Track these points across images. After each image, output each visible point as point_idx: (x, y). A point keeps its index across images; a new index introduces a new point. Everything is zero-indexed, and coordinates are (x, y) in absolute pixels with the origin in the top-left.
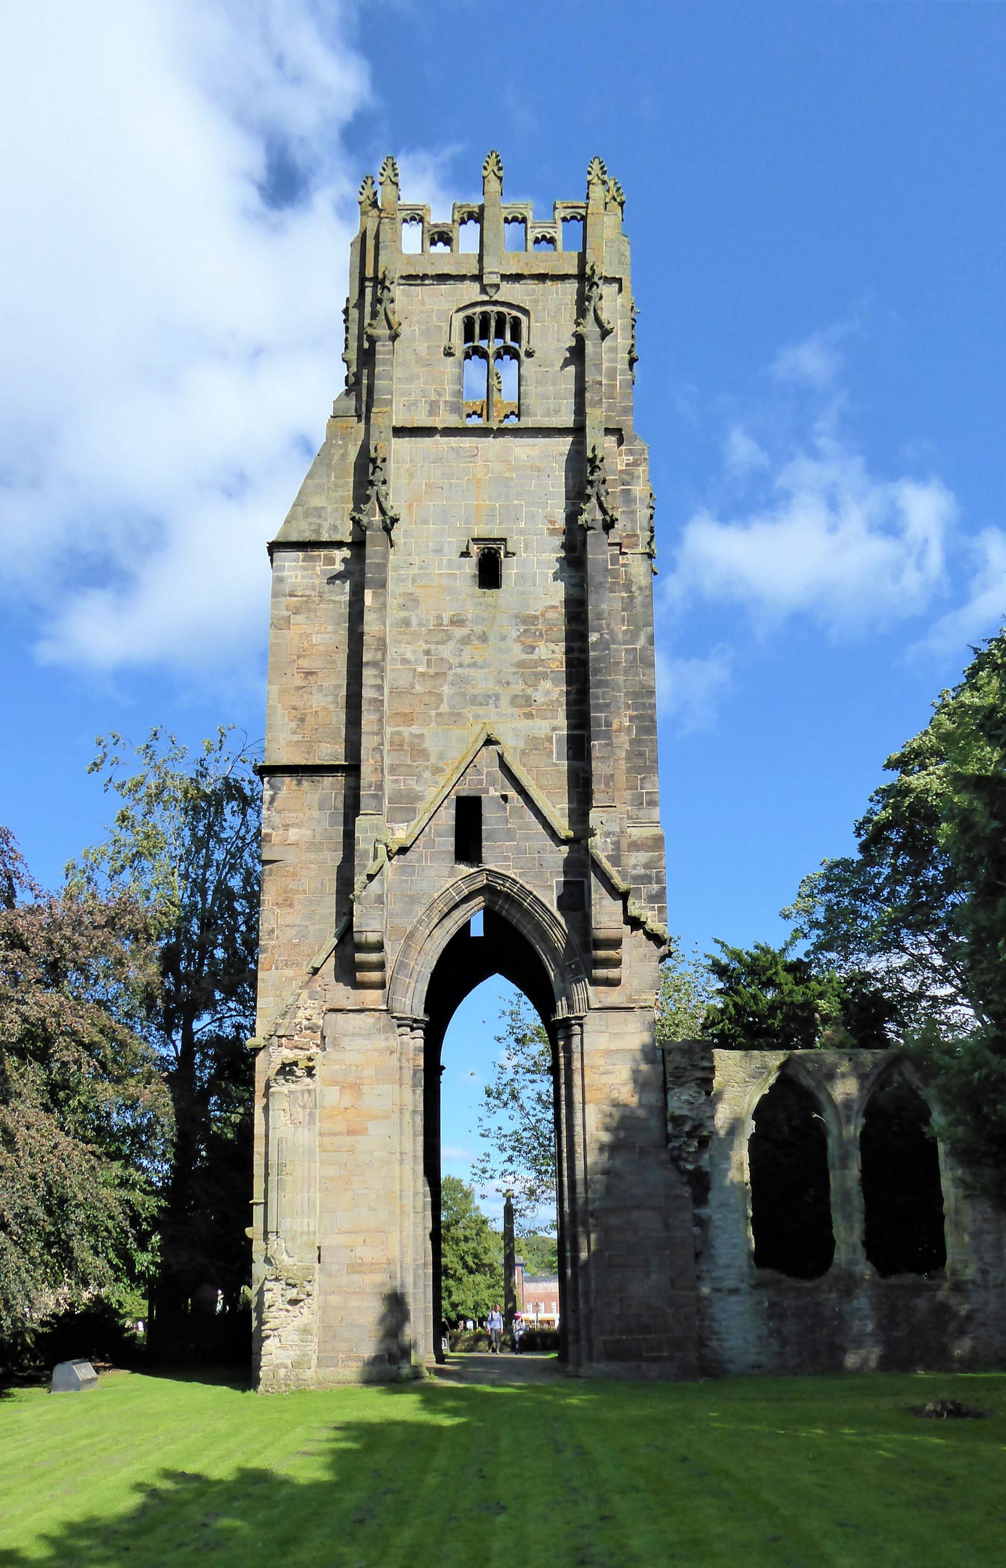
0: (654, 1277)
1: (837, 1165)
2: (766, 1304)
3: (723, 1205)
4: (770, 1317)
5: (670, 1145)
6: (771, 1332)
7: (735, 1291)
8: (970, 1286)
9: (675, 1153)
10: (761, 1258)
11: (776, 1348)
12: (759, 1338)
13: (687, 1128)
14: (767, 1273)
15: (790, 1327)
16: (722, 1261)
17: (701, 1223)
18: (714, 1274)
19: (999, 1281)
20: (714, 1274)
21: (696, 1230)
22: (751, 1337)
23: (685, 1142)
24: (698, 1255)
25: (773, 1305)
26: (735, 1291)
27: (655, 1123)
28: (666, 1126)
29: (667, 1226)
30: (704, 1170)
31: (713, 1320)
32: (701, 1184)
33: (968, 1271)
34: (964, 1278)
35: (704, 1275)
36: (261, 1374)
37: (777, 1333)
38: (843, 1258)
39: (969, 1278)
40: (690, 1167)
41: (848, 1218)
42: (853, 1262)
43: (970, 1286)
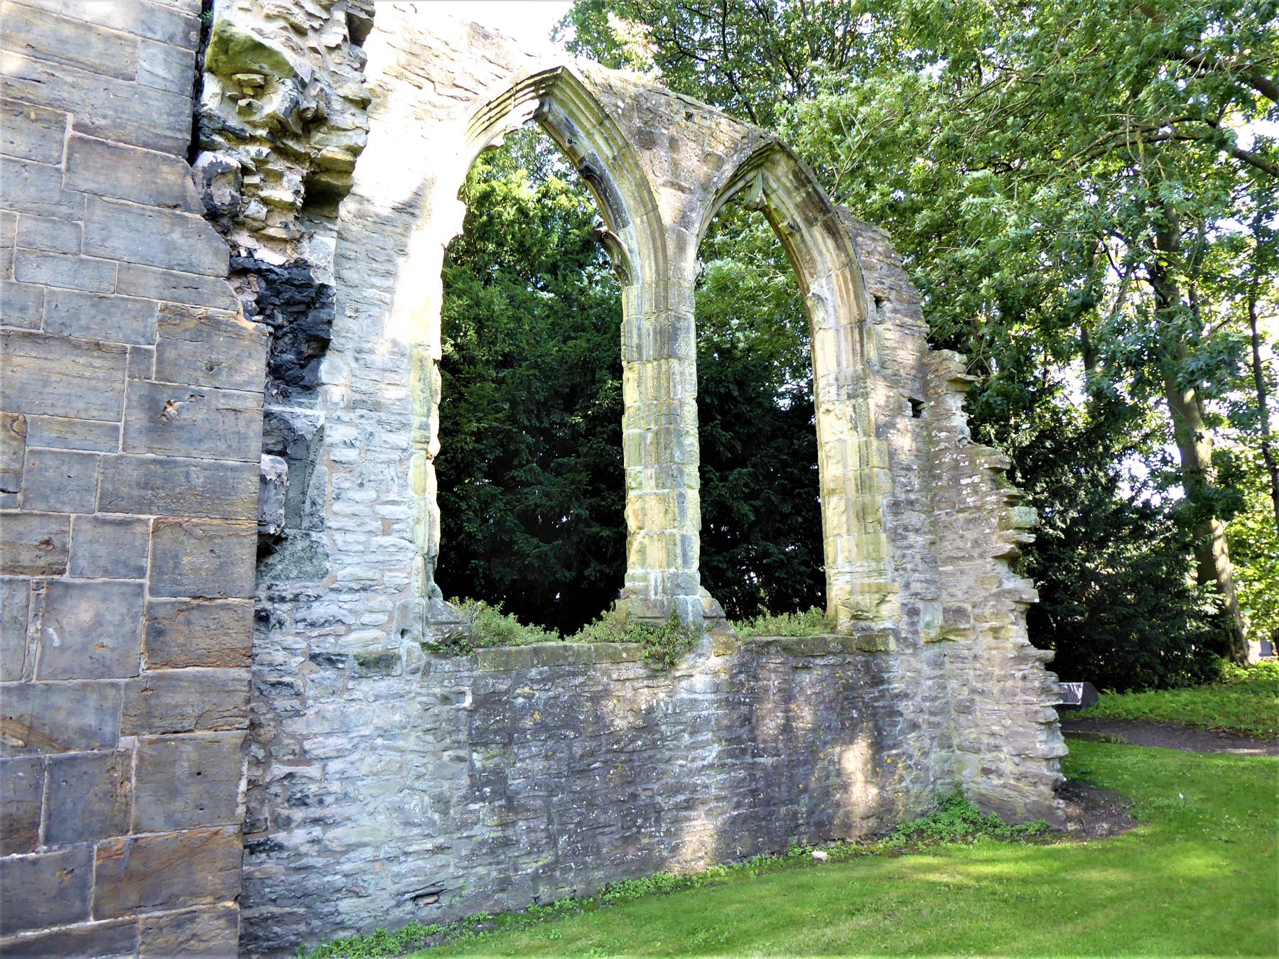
0: (82, 612)
1: (649, 350)
2: (468, 701)
3: (364, 404)
4: (478, 740)
5: (205, 158)
6: (476, 782)
7: (380, 663)
8: (893, 645)
9: (223, 194)
10: (456, 572)
11: (486, 831)
12: (442, 803)
13: (275, 103)
14: (473, 615)
15: (528, 765)
16: (346, 570)
17: (290, 445)
18: (319, 611)
19: (933, 634)
20: (319, 611)
21: (271, 465)
22: (416, 804)
23: (260, 162)
24: (267, 546)
25: (487, 702)
26: (380, 663)
27: (158, 67)
28: (198, 87)
29: (159, 423)
30: (319, 278)
31: (302, 757)
32: (299, 322)
33: (885, 609)
34: (878, 626)
35: (282, 610)
36: (622, 591)
37: (491, 785)
38: (655, 575)
39: (889, 625)
40: (271, 257)
41: (668, 476)
42: (675, 586)
43: (893, 645)
